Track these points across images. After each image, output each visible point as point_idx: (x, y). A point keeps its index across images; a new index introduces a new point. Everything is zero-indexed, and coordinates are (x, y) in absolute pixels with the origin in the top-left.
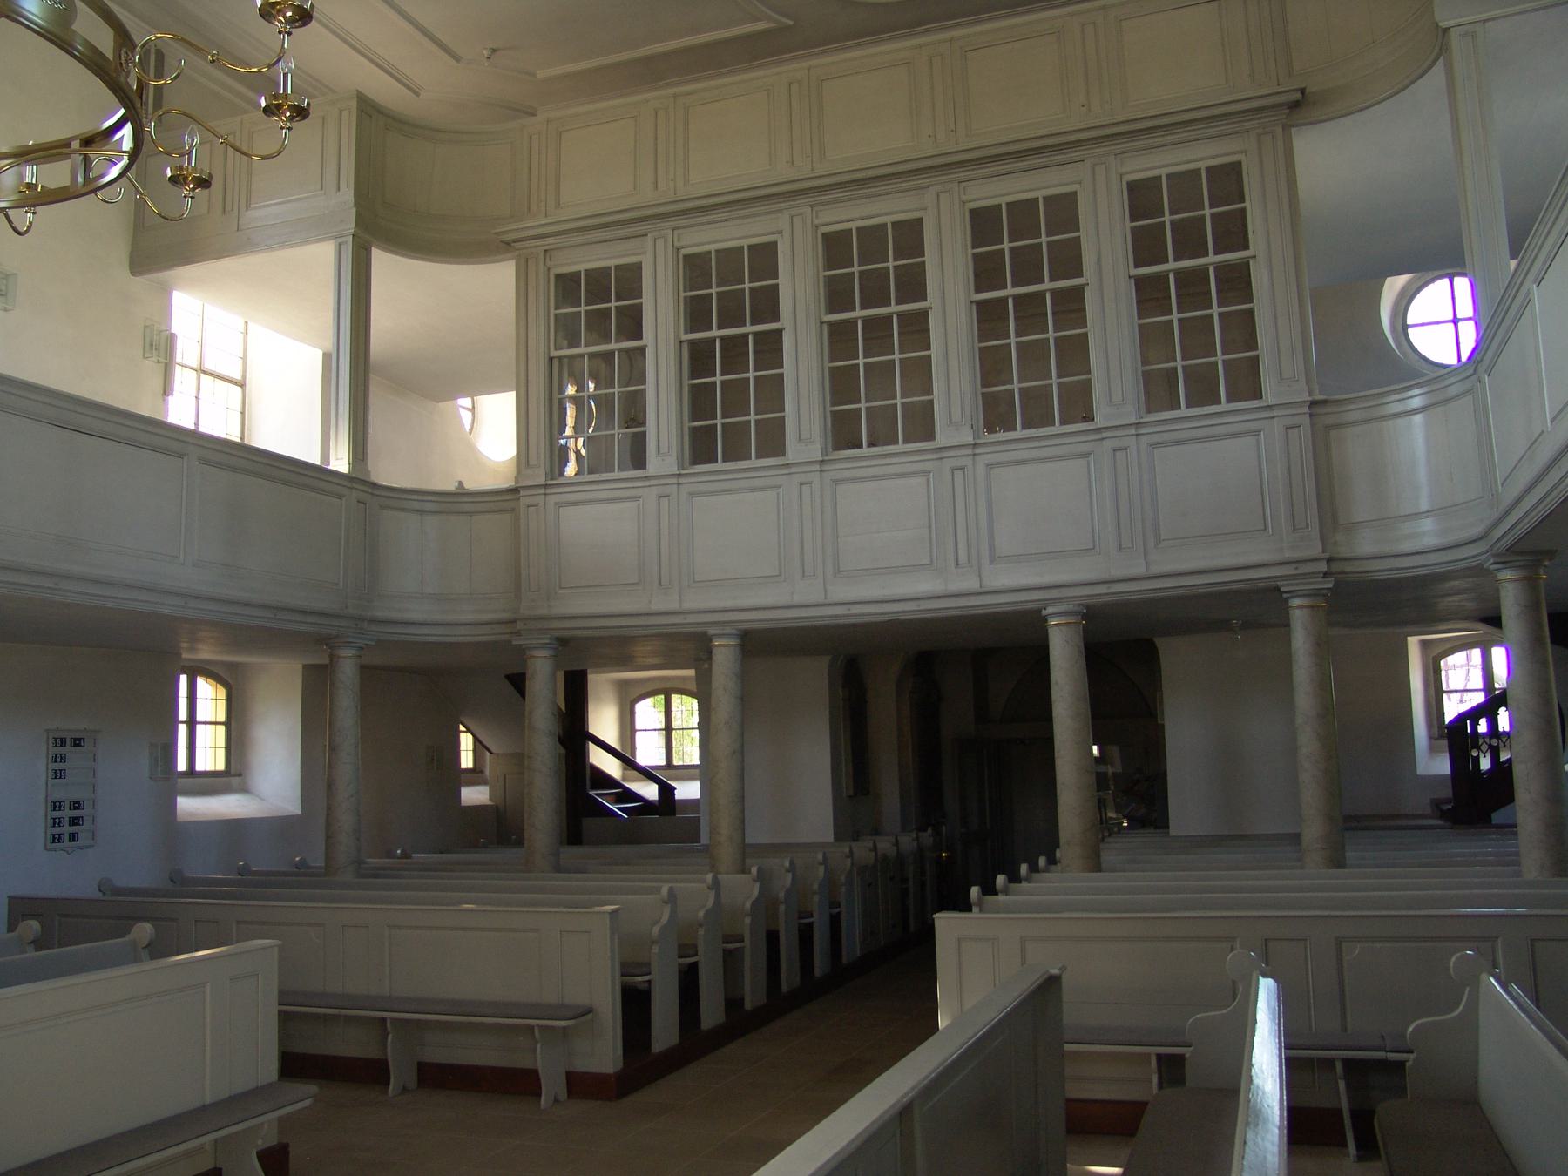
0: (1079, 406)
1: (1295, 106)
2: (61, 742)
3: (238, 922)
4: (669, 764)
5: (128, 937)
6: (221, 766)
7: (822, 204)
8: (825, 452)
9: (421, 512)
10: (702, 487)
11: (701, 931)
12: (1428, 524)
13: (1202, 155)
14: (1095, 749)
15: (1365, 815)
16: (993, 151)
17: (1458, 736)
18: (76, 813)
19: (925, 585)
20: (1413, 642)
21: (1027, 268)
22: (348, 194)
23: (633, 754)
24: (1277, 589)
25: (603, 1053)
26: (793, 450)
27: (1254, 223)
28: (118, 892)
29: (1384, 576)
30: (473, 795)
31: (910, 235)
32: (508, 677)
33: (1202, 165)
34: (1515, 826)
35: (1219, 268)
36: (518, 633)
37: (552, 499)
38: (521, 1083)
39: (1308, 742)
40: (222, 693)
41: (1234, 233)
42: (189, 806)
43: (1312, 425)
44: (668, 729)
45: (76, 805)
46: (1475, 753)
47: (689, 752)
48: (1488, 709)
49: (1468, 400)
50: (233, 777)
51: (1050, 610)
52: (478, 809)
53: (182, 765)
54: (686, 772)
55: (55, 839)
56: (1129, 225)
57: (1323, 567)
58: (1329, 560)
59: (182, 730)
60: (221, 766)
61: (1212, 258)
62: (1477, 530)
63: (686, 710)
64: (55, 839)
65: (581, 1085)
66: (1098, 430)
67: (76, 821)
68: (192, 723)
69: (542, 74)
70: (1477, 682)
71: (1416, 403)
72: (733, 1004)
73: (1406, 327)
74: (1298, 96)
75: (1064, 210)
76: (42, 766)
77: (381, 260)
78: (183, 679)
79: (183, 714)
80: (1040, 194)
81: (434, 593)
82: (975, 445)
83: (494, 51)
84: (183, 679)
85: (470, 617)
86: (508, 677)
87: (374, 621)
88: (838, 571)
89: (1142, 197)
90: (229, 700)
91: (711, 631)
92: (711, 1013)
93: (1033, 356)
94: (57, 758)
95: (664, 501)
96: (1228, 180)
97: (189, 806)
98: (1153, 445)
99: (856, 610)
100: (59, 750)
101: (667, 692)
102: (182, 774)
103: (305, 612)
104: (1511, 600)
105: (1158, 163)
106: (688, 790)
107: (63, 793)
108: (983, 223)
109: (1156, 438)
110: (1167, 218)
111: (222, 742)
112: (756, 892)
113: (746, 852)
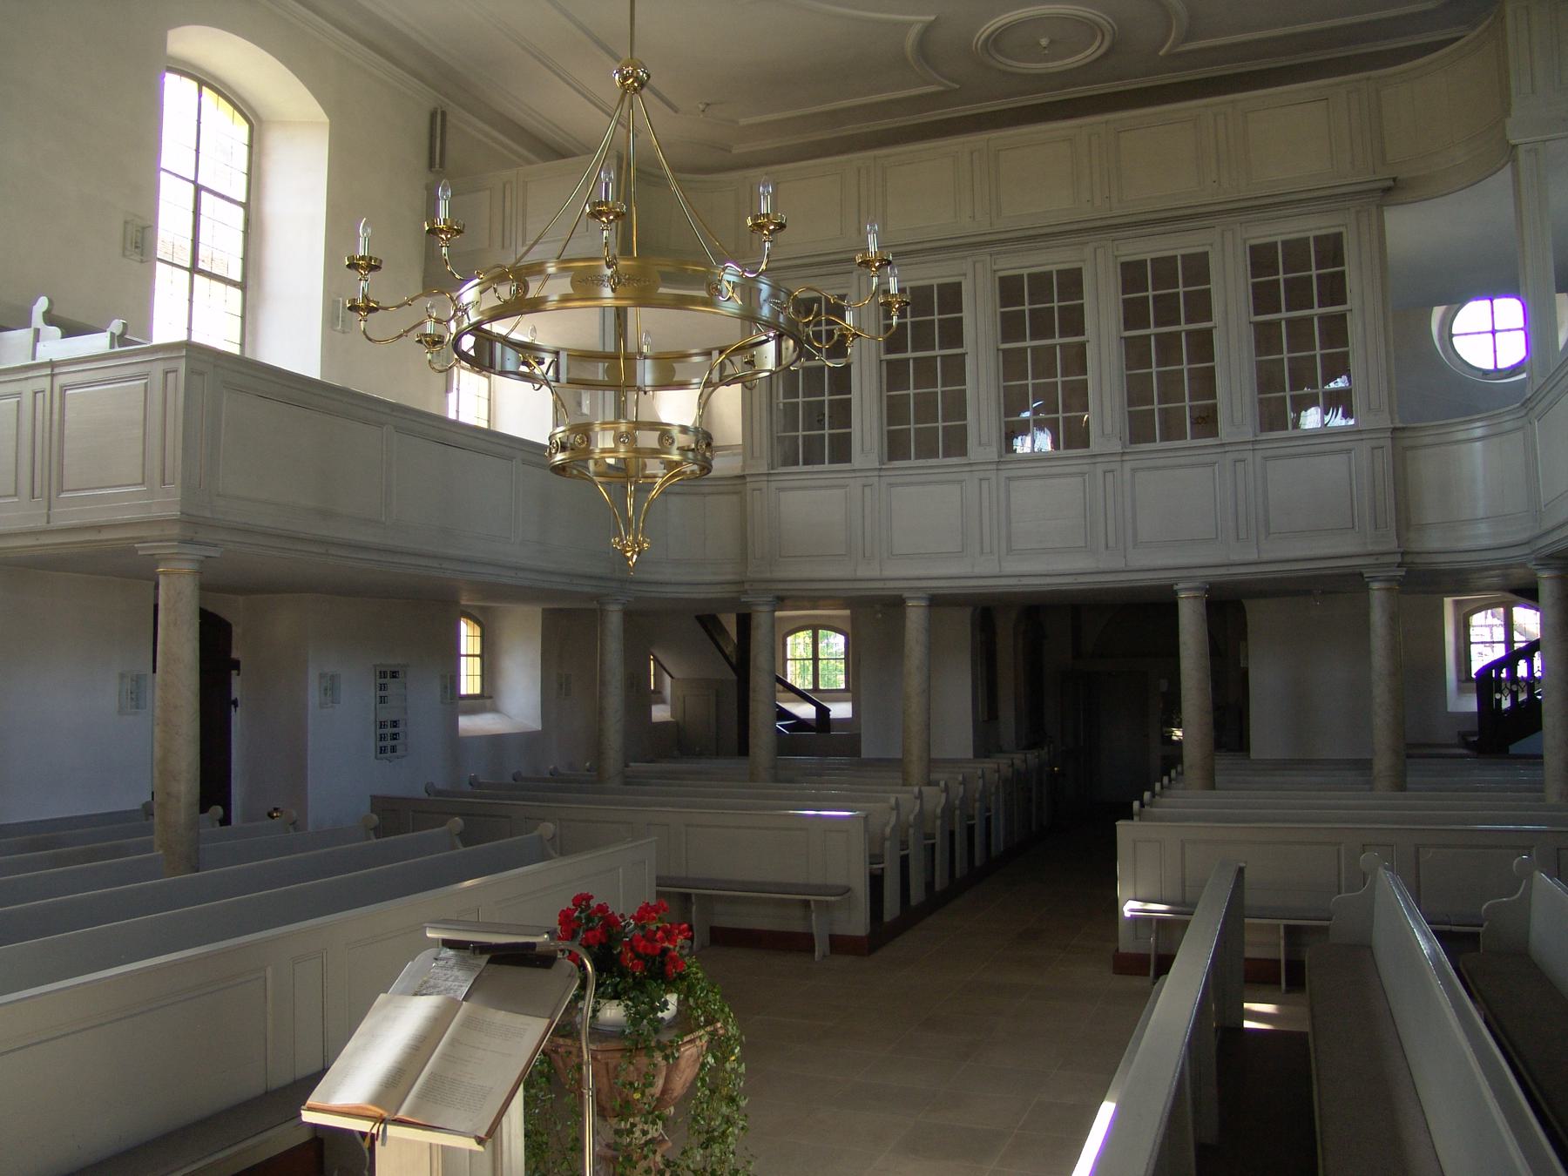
0: (1206, 422)
1: (1387, 190)
2: (383, 675)
4: (816, 689)
5: (536, 833)
6: (477, 691)
7: (999, 253)
8: (1000, 456)
10: (899, 480)
11: (911, 831)
12: (1483, 528)
13: (1310, 227)
15: (1418, 749)
16: (1143, 217)
17: (1487, 682)
18: (395, 730)
20: (1448, 602)
21: (1167, 312)
23: (785, 675)
24: (1361, 574)
25: (857, 923)
26: (975, 451)
27: (1351, 283)
28: (439, 793)
29: (1447, 567)
30: (660, 713)
31: (1072, 282)
32: (699, 618)
33: (1311, 234)
34: (1541, 757)
35: (1322, 318)
36: (745, 592)
37: (773, 485)
38: (800, 943)
39: (1381, 693)
40: (478, 631)
41: (1334, 290)
42: (469, 724)
43: (1393, 446)
44: (815, 659)
45: (395, 724)
46: (1498, 696)
47: (835, 678)
48: (1510, 660)
49: (1520, 434)
50: (486, 700)
51: (1181, 586)
52: (663, 725)
54: (835, 695)
55: (382, 750)
56: (1251, 281)
57: (1398, 559)
58: (1403, 554)
60: (477, 691)
61: (1317, 310)
62: (1524, 536)
63: (834, 644)
64: (382, 750)
65: (840, 944)
66: (1223, 445)
67: (395, 737)
69: (743, 122)
70: (1500, 634)
71: (1478, 433)
72: (930, 885)
73: (1451, 336)
74: (1391, 183)
75: (1198, 267)
76: (371, 694)
80: (1179, 253)
81: (672, 554)
82: (1254, 442)
86: (699, 618)
87: (632, 582)
88: (1010, 550)
89: (1261, 259)
90: (482, 636)
91: (906, 595)
92: (917, 894)
94: (383, 687)
95: (867, 490)
96: (1331, 250)
97: (469, 724)
98: (1266, 458)
99: (1025, 581)
100: (383, 681)
101: (814, 629)
103: (591, 577)
104: (1546, 589)
105: (1277, 231)
106: (841, 710)
107: (387, 715)
108: (1132, 274)
109: (1270, 453)
110: (1281, 276)
111: (478, 671)
112: (943, 800)
113: (931, 764)
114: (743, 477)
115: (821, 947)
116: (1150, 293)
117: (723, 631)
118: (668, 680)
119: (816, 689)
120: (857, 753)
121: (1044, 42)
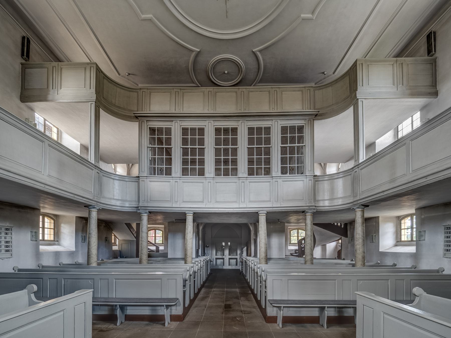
1: (316, 115)
3: (64, 279)
4: (155, 243)
7: (215, 121)
9: (113, 179)
14: (229, 243)
19: (236, 205)
21: (259, 141)
22: (93, 90)
26: (207, 175)
28: (20, 270)
37: (148, 180)
40: (52, 221)
41: (301, 139)
53: (41, 238)
59: (41, 229)
66: (272, 177)
68: (43, 228)
77: (102, 113)
78: (41, 217)
79: (41, 226)
83: (129, 74)
84: (41, 217)
85: (127, 205)
90: (54, 223)
91: (187, 212)
93: (259, 162)
96: (301, 129)
102: (41, 240)
114: (139, 177)
115: (167, 319)
116: (255, 136)
117: (132, 228)
118: (117, 240)
119: (155, 243)
120: (167, 257)
121: (226, 72)
